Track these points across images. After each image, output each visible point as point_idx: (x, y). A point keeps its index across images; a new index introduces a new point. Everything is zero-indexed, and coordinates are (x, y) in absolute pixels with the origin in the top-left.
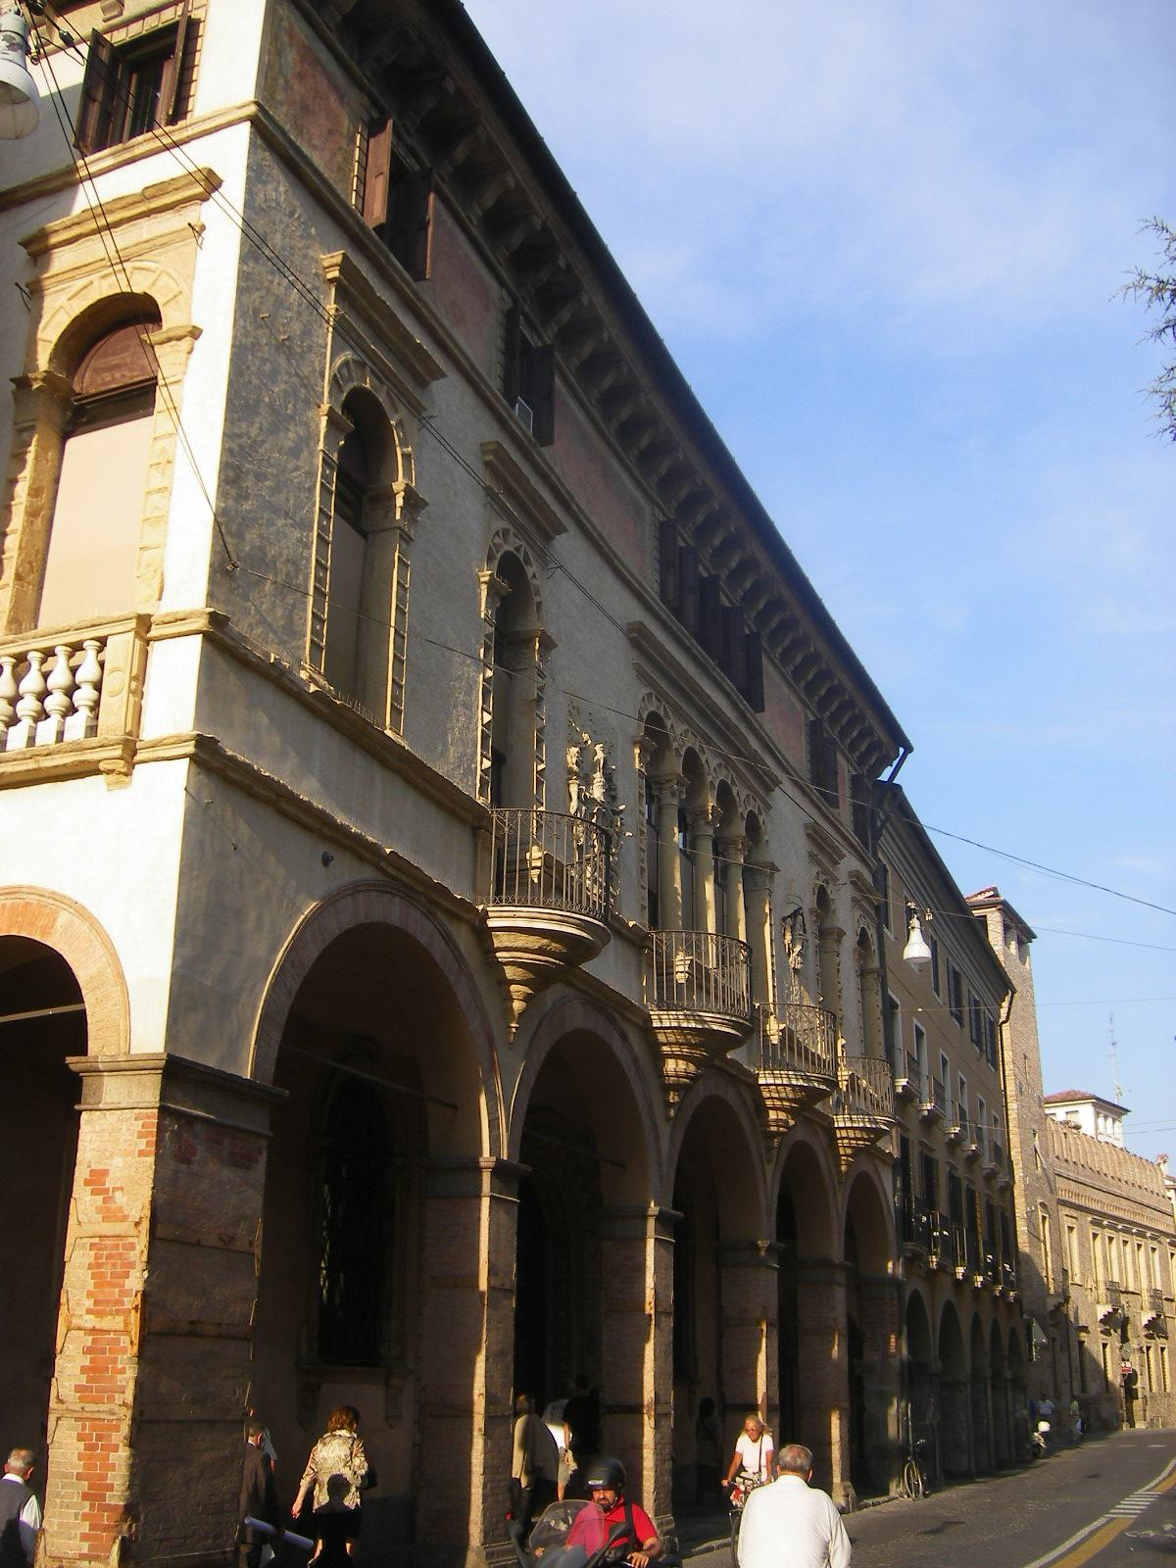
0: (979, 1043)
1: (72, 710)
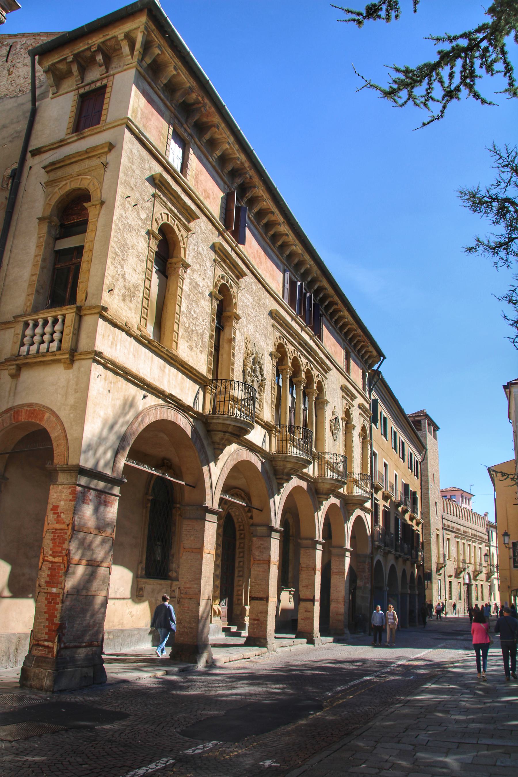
0: (411, 469)
1: (52, 341)
